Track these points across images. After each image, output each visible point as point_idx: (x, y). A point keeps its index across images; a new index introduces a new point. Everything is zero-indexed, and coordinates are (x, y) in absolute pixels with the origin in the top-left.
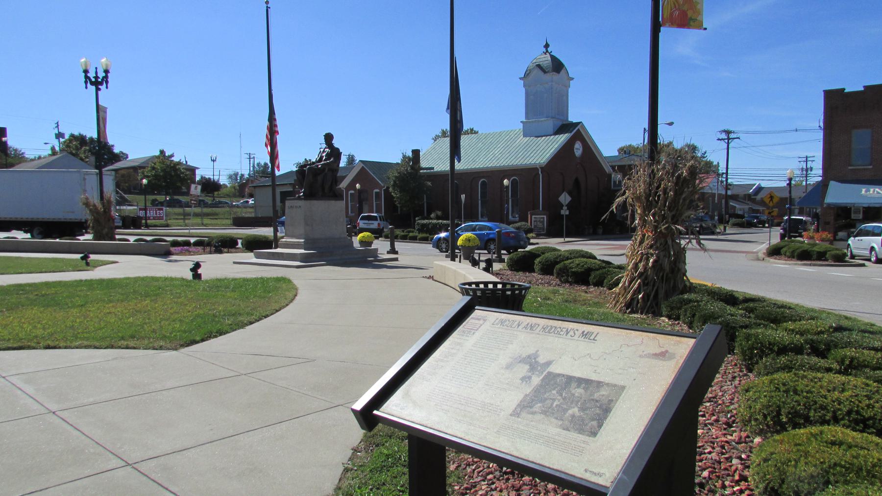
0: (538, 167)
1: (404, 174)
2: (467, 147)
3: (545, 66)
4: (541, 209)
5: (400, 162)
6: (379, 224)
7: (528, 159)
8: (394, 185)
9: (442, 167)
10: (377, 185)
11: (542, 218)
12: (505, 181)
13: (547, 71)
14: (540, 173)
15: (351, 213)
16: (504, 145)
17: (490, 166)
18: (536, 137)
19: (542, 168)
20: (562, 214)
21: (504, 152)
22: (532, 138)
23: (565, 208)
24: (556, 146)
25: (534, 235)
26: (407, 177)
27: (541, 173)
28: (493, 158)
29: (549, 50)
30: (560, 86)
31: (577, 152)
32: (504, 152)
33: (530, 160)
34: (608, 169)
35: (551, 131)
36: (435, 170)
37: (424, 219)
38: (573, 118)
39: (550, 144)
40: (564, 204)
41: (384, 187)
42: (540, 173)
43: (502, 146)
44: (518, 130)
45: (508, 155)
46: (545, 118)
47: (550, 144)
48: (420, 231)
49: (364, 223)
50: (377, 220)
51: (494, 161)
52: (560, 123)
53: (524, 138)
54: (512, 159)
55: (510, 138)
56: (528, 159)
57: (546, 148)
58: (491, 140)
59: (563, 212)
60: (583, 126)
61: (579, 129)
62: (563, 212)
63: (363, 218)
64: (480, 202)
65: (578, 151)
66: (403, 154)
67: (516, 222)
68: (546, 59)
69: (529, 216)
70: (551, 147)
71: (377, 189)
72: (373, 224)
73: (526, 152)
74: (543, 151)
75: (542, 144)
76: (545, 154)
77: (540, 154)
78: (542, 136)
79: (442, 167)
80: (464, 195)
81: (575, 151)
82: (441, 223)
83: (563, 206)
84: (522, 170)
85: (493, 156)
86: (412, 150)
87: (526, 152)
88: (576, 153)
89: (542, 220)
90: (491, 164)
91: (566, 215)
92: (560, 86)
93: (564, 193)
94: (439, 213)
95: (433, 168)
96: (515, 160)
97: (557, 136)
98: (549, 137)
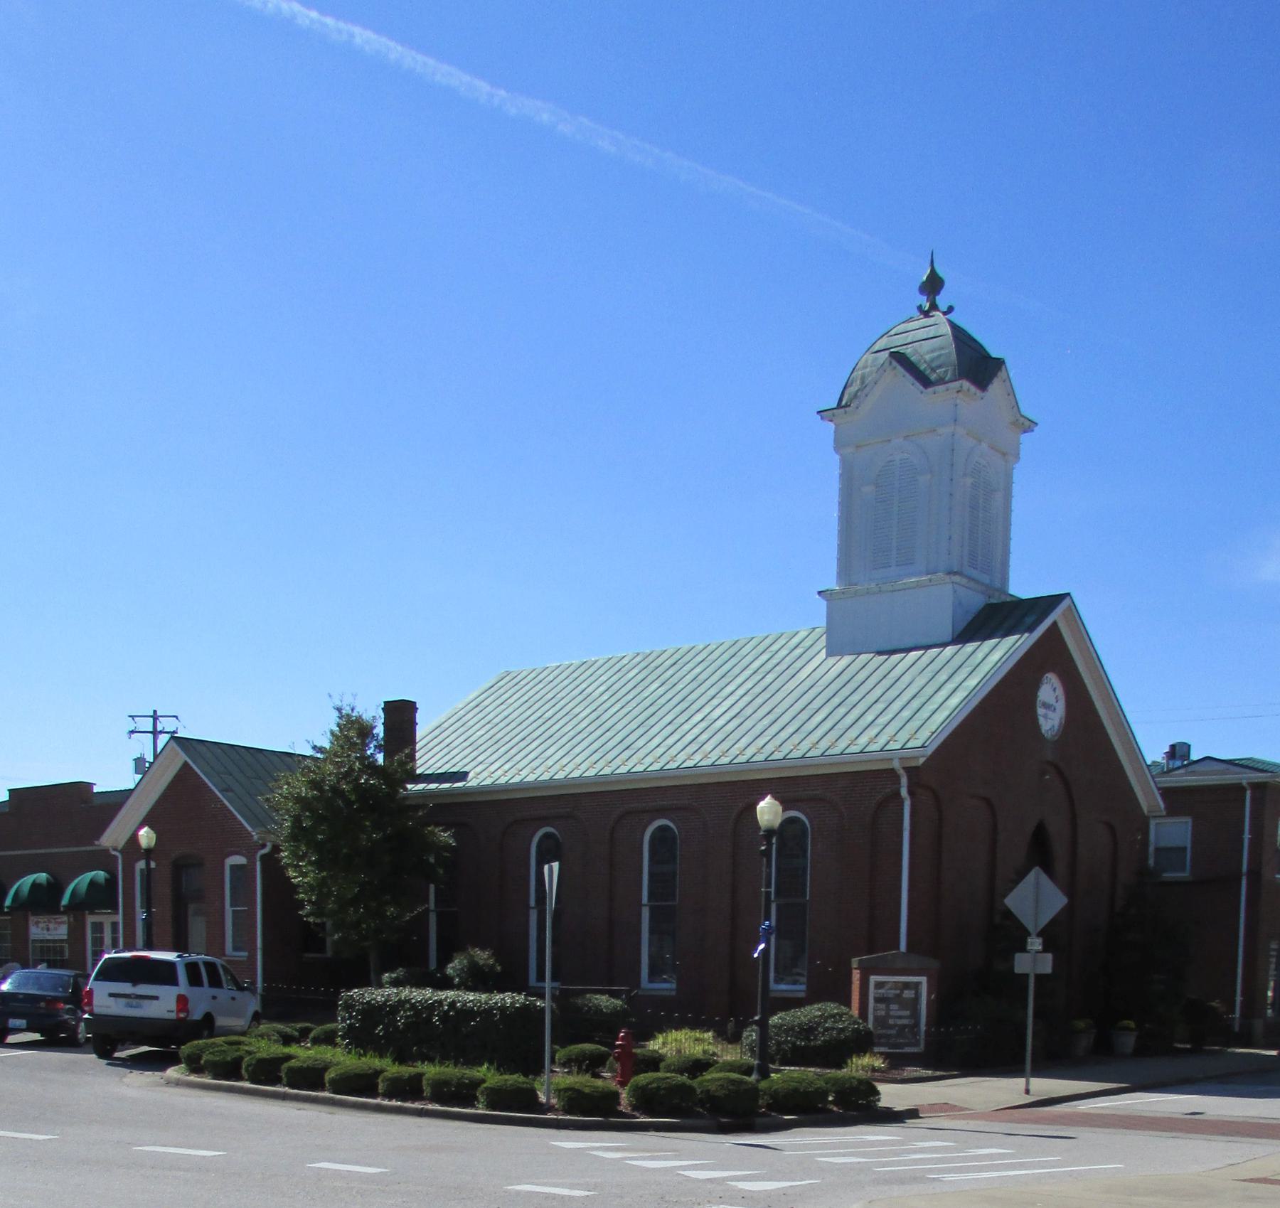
0: (896, 765)
1: (335, 790)
2: (605, 697)
3: (928, 357)
4: (903, 947)
5: (328, 747)
6: (182, 1001)
7: (853, 733)
8: (298, 834)
9: (500, 772)
10: (237, 840)
11: (907, 986)
12: (762, 804)
13: (933, 377)
14: (904, 792)
15: (236, 949)
16: (749, 685)
17: (689, 763)
18: (880, 653)
19: (911, 771)
20: (1018, 970)
21: (749, 710)
22: (864, 658)
23: (1035, 944)
24: (972, 682)
25: (879, 1063)
26: (349, 803)
27: (911, 793)
28: (704, 737)
29: (942, 301)
30: (984, 445)
31: (1045, 716)
32: (749, 710)
33: (863, 740)
34: (1148, 799)
35: (947, 632)
36: (472, 782)
37: (420, 984)
38: (1023, 585)
39: (943, 677)
40: (1030, 927)
41: (264, 846)
42: (904, 792)
43: (741, 692)
44: (803, 634)
45: (766, 722)
46: (920, 574)
47: (943, 677)
48: (360, 1039)
49: (111, 995)
50: (173, 981)
51: (708, 747)
52: (976, 601)
53: (832, 660)
54: (784, 735)
55: (774, 661)
56: (853, 733)
57: (929, 690)
58: (698, 670)
59: (1022, 963)
60: (1073, 612)
61: (1055, 624)
62: (1022, 963)
63: (113, 972)
64: (646, 913)
65: (1051, 714)
66: (339, 710)
67: (798, 1003)
68: (931, 332)
69: (856, 975)
70: (950, 686)
71: (237, 853)
72: (156, 998)
73: (842, 710)
74: (916, 704)
75: (906, 678)
76: (924, 714)
77: (906, 714)
78: (908, 650)
79: (500, 772)
80: (556, 865)
81: (1041, 711)
82: (452, 1005)
83: (1025, 933)
84: (828, 780)
85: (703, 725)
86: (386, 703)
87: (842, 710)
88: (1041, 720)
89: (908, 994)
90: (697, 757)
91: (1039, 978)
92: (984, 445)
93: (1031, 877)
94: (483, 956)
95: (462, 776)
96: (796, 739)
97: (970, 647)
98: (934, 651)
